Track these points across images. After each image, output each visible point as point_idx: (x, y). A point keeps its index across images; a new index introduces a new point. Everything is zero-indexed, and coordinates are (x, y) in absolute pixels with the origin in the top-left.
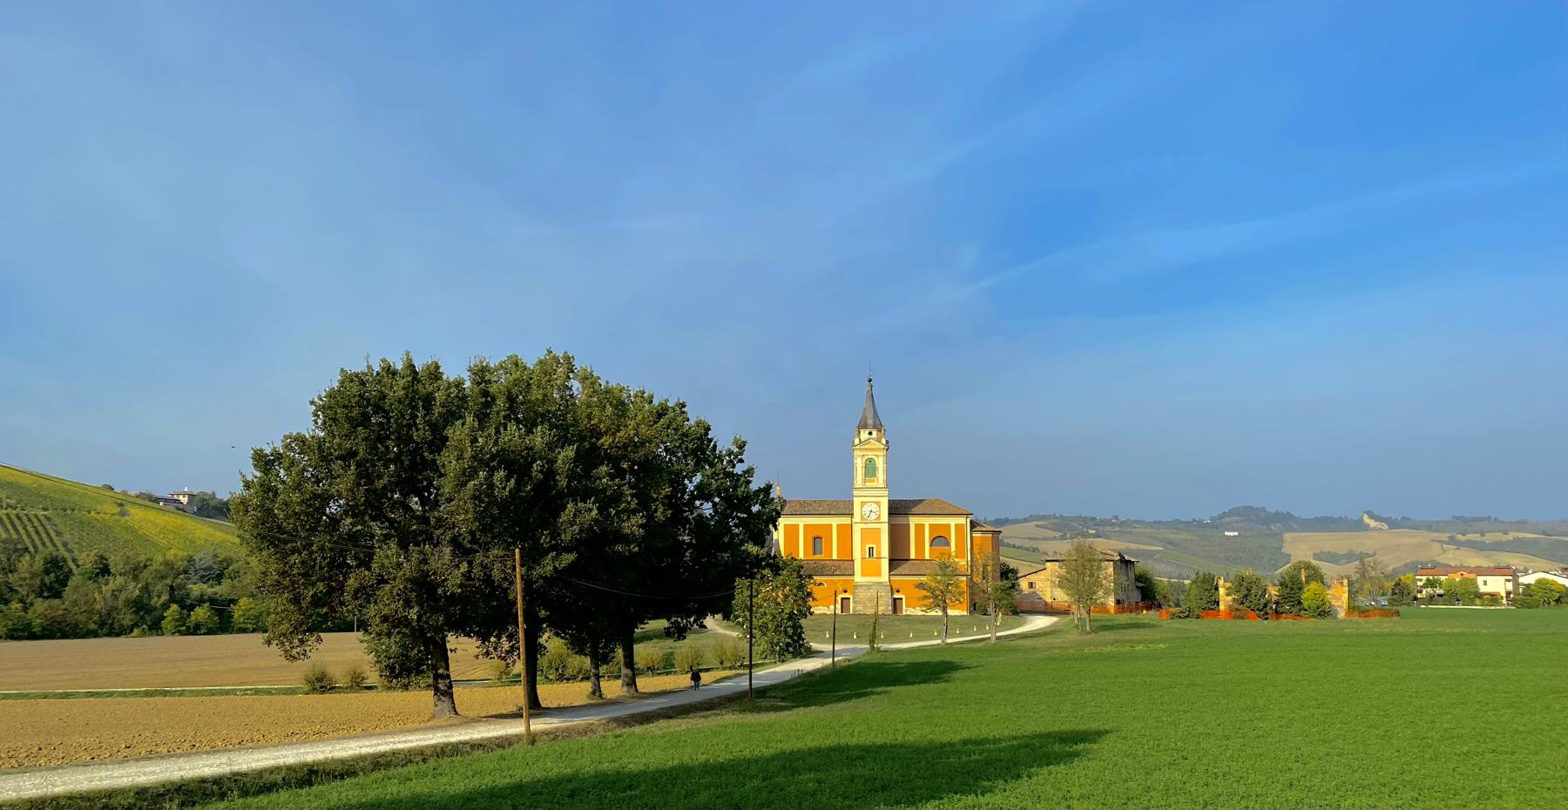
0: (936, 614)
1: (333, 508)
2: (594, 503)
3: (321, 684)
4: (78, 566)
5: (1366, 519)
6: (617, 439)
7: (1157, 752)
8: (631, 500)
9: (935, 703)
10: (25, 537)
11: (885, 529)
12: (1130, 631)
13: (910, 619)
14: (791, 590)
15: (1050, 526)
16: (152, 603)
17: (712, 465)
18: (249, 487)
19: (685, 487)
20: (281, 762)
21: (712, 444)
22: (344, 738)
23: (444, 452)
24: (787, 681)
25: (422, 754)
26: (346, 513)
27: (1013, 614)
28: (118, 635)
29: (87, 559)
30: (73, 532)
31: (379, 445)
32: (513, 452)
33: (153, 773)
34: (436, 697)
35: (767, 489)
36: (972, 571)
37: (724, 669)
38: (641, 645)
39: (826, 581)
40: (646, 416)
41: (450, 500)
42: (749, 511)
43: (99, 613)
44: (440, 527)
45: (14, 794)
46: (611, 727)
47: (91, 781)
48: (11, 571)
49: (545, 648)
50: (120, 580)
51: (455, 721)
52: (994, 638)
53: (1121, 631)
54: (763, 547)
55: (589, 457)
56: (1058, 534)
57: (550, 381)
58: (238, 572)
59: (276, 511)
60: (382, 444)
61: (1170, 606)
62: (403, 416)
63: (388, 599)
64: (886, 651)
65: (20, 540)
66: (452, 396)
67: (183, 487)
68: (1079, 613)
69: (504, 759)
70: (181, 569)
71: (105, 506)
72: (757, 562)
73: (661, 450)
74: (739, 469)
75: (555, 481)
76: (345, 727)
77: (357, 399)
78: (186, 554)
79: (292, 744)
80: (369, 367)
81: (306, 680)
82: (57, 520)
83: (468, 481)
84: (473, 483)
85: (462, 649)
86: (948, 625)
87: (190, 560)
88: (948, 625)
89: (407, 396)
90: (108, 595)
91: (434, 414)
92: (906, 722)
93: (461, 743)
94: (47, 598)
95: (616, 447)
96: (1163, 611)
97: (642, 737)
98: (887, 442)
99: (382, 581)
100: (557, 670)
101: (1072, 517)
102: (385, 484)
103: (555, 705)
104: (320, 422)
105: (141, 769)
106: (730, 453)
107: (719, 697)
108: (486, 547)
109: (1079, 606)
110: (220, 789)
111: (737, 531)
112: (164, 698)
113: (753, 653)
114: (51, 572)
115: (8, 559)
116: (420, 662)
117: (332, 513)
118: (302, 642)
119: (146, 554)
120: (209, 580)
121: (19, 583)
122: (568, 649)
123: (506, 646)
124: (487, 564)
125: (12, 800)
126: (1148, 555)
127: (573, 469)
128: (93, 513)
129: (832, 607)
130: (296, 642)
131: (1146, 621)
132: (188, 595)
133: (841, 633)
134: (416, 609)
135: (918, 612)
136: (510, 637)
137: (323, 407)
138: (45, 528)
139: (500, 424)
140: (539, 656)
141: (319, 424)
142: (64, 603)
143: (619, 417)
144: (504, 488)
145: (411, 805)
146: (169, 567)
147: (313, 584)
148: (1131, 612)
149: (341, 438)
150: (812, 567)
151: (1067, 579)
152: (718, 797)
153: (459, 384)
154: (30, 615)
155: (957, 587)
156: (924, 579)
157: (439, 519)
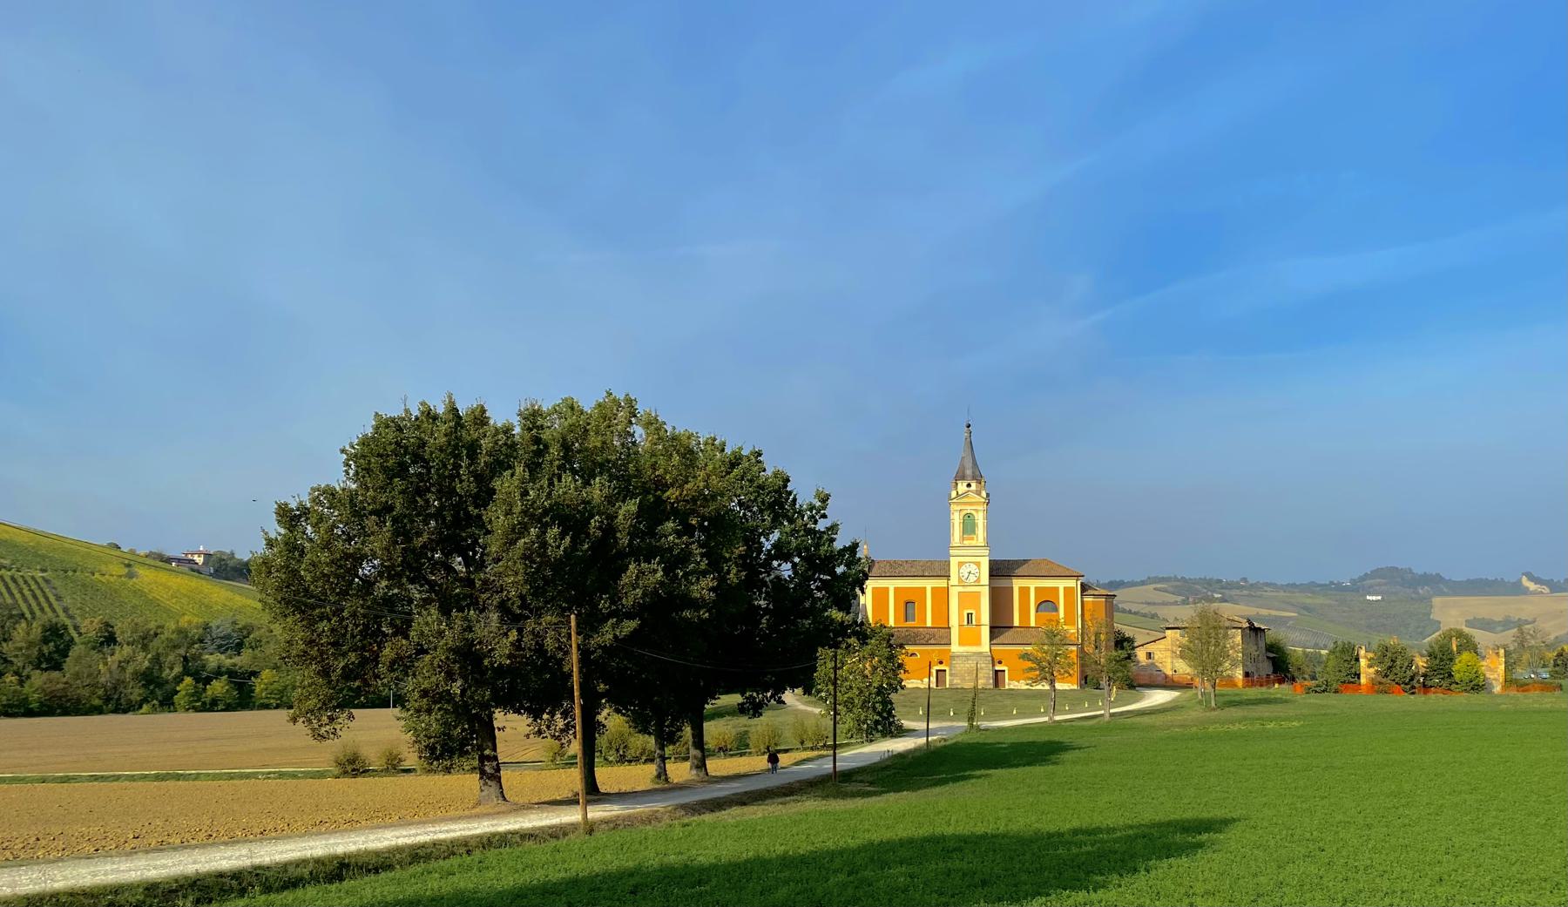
1: (366, 569)
2: (659, 564)
3: (353, 767)
4: (80, 634)
5: (1525, 582)
6: (685, 492)
7: (1290, 842)
9: (1042, 788)
10: (21, 602)
11: (985, 592)
13: (1013, 694)
14: (880, 661)
16: (163, 675)
17: (791, 521)
19: (761, 545)
20: (308, 854)
21: (791, 497)
22: (379, 827)
24: (875, 763)
25: (466, 845)
26: (381, 574)
27: (1129, 688)
28: (125, 711)
29: (90, 627)
30: (75, 596)
32: (568, 506)
34: (482, 781)
35: (854, 548)
36: (1083, 640)
37: (805, 749)
38: (712, 723)
40: (717, 466)
41: (497, 560)
43: (104, 686)
44: (487, 590)
45: (9, 890)
47: (95, 876)
49: (604, 726)
50: (127, 650)
51: (503, 808)
52: (1108, 715)
53: (1250, 707)
54: (848, 613)
55: (654, 512)
56: (1180, 598)
57: (609, 427)
58: (260, 641)
59: (302, 573)
60: (421, 497)
61: (1305, 679)
62: (445, 466)
64: (986, 730)
66: (500, 443)
67: (198, 548)
68: (1203, 687)
70: (197, 637)
71: (111, 567)
72: (842, 630)
74: (822, 525)
75: (616, 539)
76: (380, 814)
77: (393, 446)
78: (201, 620)
79: (319, 834)
80: (407, 411)
81: (336, 762)
82: (57, 583)
84: (523, 540)
85: (511, 727)
86: (1055, 700)
88: (1055, 700)
89: (450, 444)
90: (115, 667)
92: (1009, 809)
94: (46, 670)
98: (988, 495)
100: (617, 750)
104: (351, 472)
105: (151, 863)
106: (812, 508)
109: (1203, 679)
111: (819, 595)
112: (177, 782)
113: (838, 731)
114: (50, 641)
116: (464, 742)
120: (227, 649)
121: (14, 653)
122: (630, 727)
126: (1282, 621)
127: (635, 525)
128: (97, 575)
129: (926, 680)
130: (325, 718)
131: (1279, 696)
132: (204, 666)
133: (936, 709)
134: (459, 683)
135: (1022, 685)
136: (565, 714)
137: (356, 456)
139: (554, 475)
140: (597, 735)
141: (351, 475)
142: (64, 676)
144: (558, 547)
146: (182, 635)
148: (1261, 686)
149: (374, 491)
151: (1189, 649)
153: (507, 430)
154: (27, 689)
155: (1066, 658)
156: (1029, 648)
157: (485, 582)
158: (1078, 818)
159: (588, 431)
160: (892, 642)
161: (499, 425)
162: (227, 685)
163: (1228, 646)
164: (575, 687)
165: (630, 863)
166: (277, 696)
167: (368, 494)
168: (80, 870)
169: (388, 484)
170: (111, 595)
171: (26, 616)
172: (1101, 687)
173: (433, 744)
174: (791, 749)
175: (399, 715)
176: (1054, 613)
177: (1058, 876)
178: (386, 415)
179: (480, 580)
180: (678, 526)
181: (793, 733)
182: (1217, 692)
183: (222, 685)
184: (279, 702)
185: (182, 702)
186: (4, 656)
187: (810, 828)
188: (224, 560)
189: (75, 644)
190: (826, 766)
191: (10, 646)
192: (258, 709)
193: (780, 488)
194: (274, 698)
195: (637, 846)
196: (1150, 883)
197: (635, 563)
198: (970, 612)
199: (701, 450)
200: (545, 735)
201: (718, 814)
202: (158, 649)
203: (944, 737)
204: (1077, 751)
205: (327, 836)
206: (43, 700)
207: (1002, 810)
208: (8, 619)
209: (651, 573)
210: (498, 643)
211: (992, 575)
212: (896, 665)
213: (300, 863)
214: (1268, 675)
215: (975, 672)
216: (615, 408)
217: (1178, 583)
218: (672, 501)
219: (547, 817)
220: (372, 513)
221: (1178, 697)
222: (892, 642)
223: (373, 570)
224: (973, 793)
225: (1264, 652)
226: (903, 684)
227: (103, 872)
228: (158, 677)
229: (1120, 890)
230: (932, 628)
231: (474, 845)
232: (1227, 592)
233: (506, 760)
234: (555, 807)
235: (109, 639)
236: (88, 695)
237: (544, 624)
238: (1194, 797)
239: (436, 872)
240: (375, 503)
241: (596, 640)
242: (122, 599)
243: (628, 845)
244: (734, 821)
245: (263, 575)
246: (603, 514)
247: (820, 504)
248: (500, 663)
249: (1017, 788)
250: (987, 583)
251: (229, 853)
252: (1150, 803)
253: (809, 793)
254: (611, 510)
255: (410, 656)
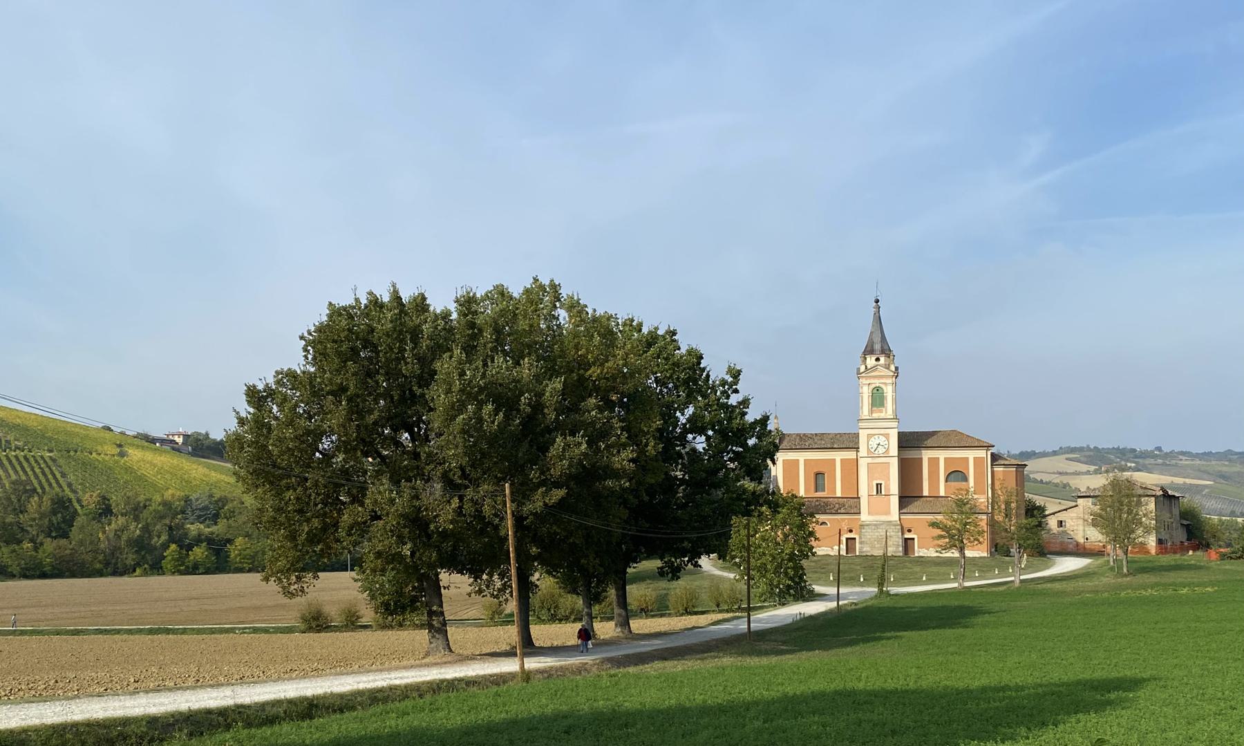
0: (952, 555)
1: (325, 444)
2: (583, 437)
3: (316, 622)
4: (82, 506)
6: (606, 370)
7: (1200, 701)
8: (621, 434)
9: (951, 649)
10: (32, 478)
12: (1172, 574)
13: (922, 561)
14: (791, 529)
15: (1082, 459)
16: (152, 543)
17: (705, 396)
18: (243, 423)
19: (677, 420)
20: (282, 696)
21: (705, 374)
22: (342, 674)
23: (434, 386)
26: (338, 449)
28: (122, 574)
29: (90, 499)
31: (370, 381)
32: (501, 385)
34: (430, 634)
35: (765, 420)
36: (993, 508)
37: (721, 612)
38: (634, 586)
39: (829, 520)
40: (635, 345)
41: (439, 435)
42: (744, 445)
47: (106, 711)
49: (537, 586)
50: (121, 520)
51: (450, 659)
52: (1018, 581)
53: (1163, 573)
54: (760, 483)
55: (577, 390)
56: (1092, 468)
57: (536, 311)
58: (234, 512)
59: (270, 448)
60: (372, 379)
61: (1220, 547)
62: (391, 349)
63: (381, 535)
64: (896, 595)
65: (29, 482)
66: (439, 328)
68: (1114, 553)
69: (499, 695)
70: (179, 509)
71: (106, 448)
73: (651, 381)
74: (734, 400)
75: (544, 414)
76: (342, 664)
77: (346, 333)
78: (183, 494)
79: (291, 679)
80: (357, 300)
81: (302, 618)
82: (61, 462)
83: (456, 416)
84: (462, 416)
85: (455, 584)
87: (187, 500)
89: (395, 330)
90: (111, 535)
91: (421, 347)
92: (918, 667)
93: (455, 679)
94: (55, 538)
95: (605, 378)
97: (637, 677)
98: (897, 368)
100: (549, 610)
101: (1109, 449)
102: (376, 420)
103: (549, 645)
104: (310, 357)
105: (151, 701)
106: (724, 383)
108: (476, 483)
109: (1115, 546)
110: (226, 721)
111: (732, 466)
112: (167, 636)
113: (752, 595)
115: (19, 500)
116: (414, 600)
117: (325, 449)
118: (299, 578)
120: (205, 520)
121: (29, 523)
122: (560, 588)
123: (499, 584)
126: (1197, 489)
128: (94, 455)
129: (836, 548)
131: (1193, 562)
132: (186, 534)
133: (846, 575)
134: (409, 546)
135: (932, 553)
136: (502, 576)
137: (314, 341)
140: (531, 595)
141: (310, 359)
142: (71, 543)
143: (608, 346)
144: (493, 422)
145: (410, 737)
146: (167, 507)
147: (308, 520)
148: (1175, 553)
149: (331, 373)
150: (813, 504)
151: (1101, 516)
153: (446, 315)
154: (40, 555)
155: (976, 526)
156: (940, 517)
157: (429, 455)
158: (987, 676)
159: (517, 315)
162: (207, 551)
163: (1141, 513)
164: (511, 549)
166: (250, 561)
168: (93, 706)
170: (106, 471)
172: (1011, 554)
173: (388, 600)
175: (356, 577)
176: (964, 483)
177: (966, 728)
179: (425, 453)
180: (599, 401)
181: (709, 597)
182: (1128, 559)
183: (202, 551)
185: (169, 566)
186: (21, 526)
188: (200, 440)
189: (79, 515)
191: (26, 517)
192: (233, 573)
193: (694, 365)
194: (246, 563)
195: (569, 692)
196: (1058, 736)
197: (561, 436)
198: (879, 482)
199: (620, 331)
200: (484, 594)
201: (641, 667)
202: (147, 519)
203: (855, 601)
205: (297, 681)
209: (576, 445)
212: (807, 533)
213: (277, 703)
214: (1181, 542)
215: (884, 540)
217: (1092, 453)
218: (594, 379)
219: (488, 666)
220: (331, 393)
221: (1090, 564)
224: (883, 652)
225: (1179, 519)
226: (814, 551)
228: (148, 544)
229: (1027, 741)
230: (842, 498)
232: (1140, 460)
233: (451, 618)
235: (105, 511)
236: (90, 559)
237: (482, 492)
239: (393, 712)
241: (528, 508)
242: (115, 476)
246: (532, 391)
247: (732, 379)
248: (445, 527)
249: (928, 649)
250: (897, 455)
255: (365, 523)
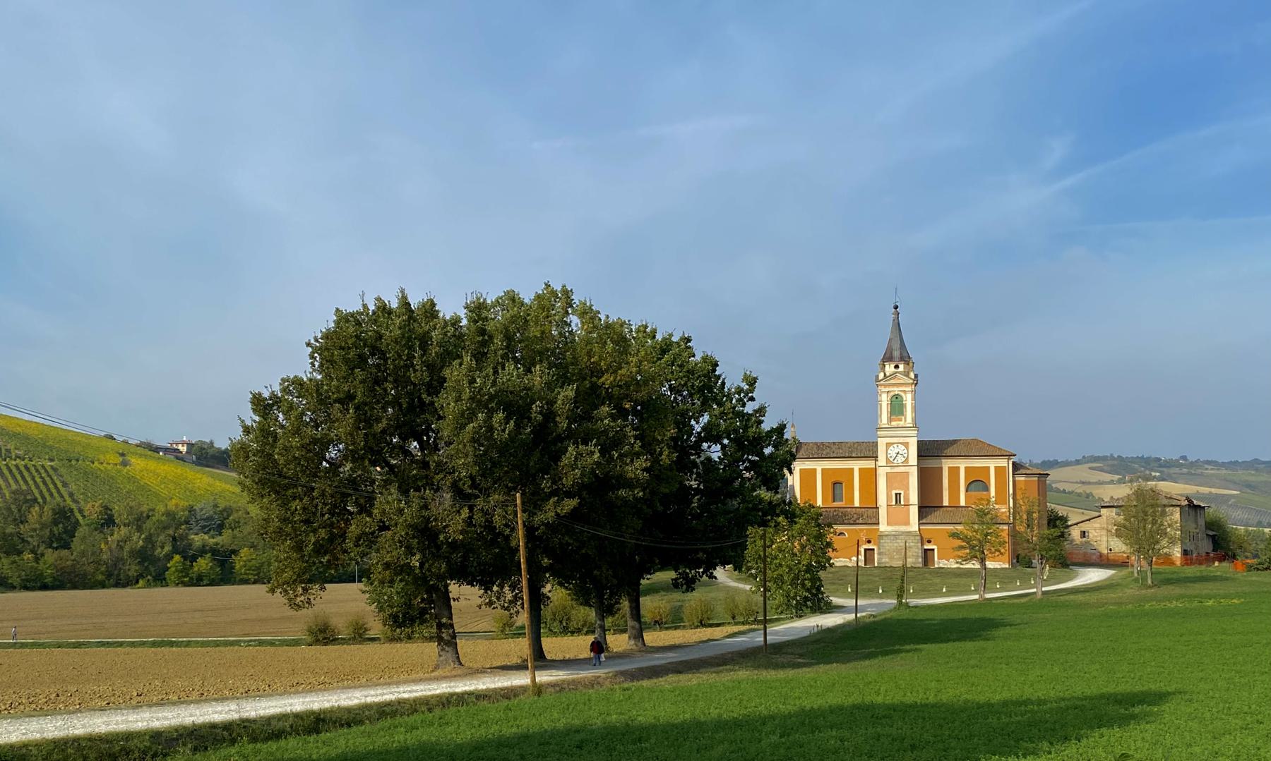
0: (973, 566)
1: (332, 453)
2: (595, 445)
3: (323, 635)
4: (84, 517)
6: (619, 378)
7: (1226, 715)
8: (635, 442)
9: (972, 662)
10: (33, 487)
11: (914, 472)
12: (1197, 586)
13: (942, 572)
14: (808, 540)
15: (1106, 468)
16: (156, 553)
17: (720, 404)
18: (249, 432)
19: (692, 428)
23: (443, 394)
24: (804, 637)
25: (427, 704)
26: (345, 458)
27: (1063, 567)
28: (124, 586)
29: (92, 509)
30: (78, 483)
31: (378, 388)
32: (512, 393)
33: (166, 718)
34: (440, 647)
35: (781, 429)
37: (736, 624)
38: (648, 598)
39: (846, 530)
40: (649, 352)
41: (449, 444)
42: (761, 454)
43: (106, 563)
44: (441, 471)
45: (38, 735)
46: (618, 680)
47: (108, 725)
48: (22, 522)
49: (548, 598)
50: (124, 531)
51: (459, 672)
52: (1040, 593)
53: (1188, 584)
54: (777, 493)
55: (590, 397)
56: (1116, 477)
57: (548, 317)
58: (239, 522)
59: (276, 457)
60: (380, 386)
61: (1247, 557)
62: (400, 356)
64: (916, 607)
66: (449, 334)
67: (180, 434)
68: (1139, 564)
69: (510, 710)
70: (183, 519)
72: (772, 509)
74: (750, 408)
75: (555, 423)
76: (349, 677)
77: (354, 339)
78: (187, 504)
79: (297, 692)
80: (365, 306)
82: (62, 471)
83: (466, 424)
85: (465, 596)
86: (987, 578)
87: (191, 510)
88: (987, 578)
89: (403, 337)
90: (114, 546)
91: (431, 354)
92: (938, 681)
94: (56, 549)
95: (617, 386)
96: (1239, 562)
97: (651, 691)
98: (916, 376)
99: (383, 528)
100: (561, 622)
102: (384, 428)
103: (561, 658)
104: (317, 364)
105: (155, 715)
106: (739, 391)
107: (732, 653)
108: (486, 493)
109: (1139, 557)
111: (748, 475)
112: (171, 649)
113: (768, 607)
114: (59, 523)
115: (19, 510)
116: (423, 612)
117: (332, 458)
119: (148, 505)
120: (210, 530)
121: (29, 534)
122: (572, 599)
123: (509, 595)
124: (488, 510)
125: (37, 740)
127: (573, 410)
128: (96, 464)
130: (300, 589)
131: (1219, 573)
132: (190, 545)
133: (864, 587)
134: (418, 557)
135: (952, 564)
136: (513, 588)
137: (320, 348)
138: (52, 479)
139: (498, 363)
140: (542, 607)
141: (316, 366)
142: (72, 554)
143: (621, 353)
144: (504, 431)
147: (315, 531)
148: (1201, 564)
149: (338, 380)
150: (831, 514)
151: (1125, 527)
152: (732, 752)
153: (455, 322)
154: (41, 566)
155: (997, 536)
156: (960, 527)
157: (439, 464)
160: (820, 521)
161: (448, 318)
163: (1166, 523)
164: (522, 560)
165: (576, 721)
166: (255, 572)
167: (333, 383)
168: (95, 720)
169: (350, 374)
171: (39, 500)
172: (1033, 565)
173: (397, 612)
174: (723, 623)
175: (364, 589)
177: (987, 742)
178: (346, 310)
179: (434, 461)
180: (613, 410)
184: (256, 577)
185: (173, 577)
186: (22, 536)
187: (742, 694)
188: (204, 449)
189: (80, 525)
190: (758, 639)
191: (26, 527)
192: (238, 584)
193: (709, 373)
194: (252, 574)
195: (582, 706)
198: (898, 492)
199: (633, 337)
200: (495, 606)
203: (873, 613)
204: (1008, 627)
205: (304, 695)
206: (55, 575)
207: (932, 681)
208: (23, 503)
209: (588, 454)
210: (452, 520)
211: (920, 456)
212: (825, 543)
213: (282, 717)
214: (1207, 553)
215: (904, 551)
216: (553, 299)
217: (1116, 462)
218: (607, 386)
219: (499, 680)
220: (336, 401)
221: (1113, 575)
222: (820, 521)
223: (338, 455)
225: (1204, 529)
226: (831, 562)
227: (114, 722)
228: (151, 555)
229: (1049, 756)
231: (434, 704)
233: (461, 630)
234: (505, 671)
235: (108, 521)
236: (92, 571)
237: (492, 502)
238: (1128, 672)
240: (339, 392)
241: (539, 518)
242: (118, 486)
243: (573, 706)
244: (670, 686)
245: (241, 459)
246: (543, 399)
247: (748, 387)
251: (220, 709)
252: (1083, 677)
253: (741, 664)
254: (551, 396)
255: (373, 533)
